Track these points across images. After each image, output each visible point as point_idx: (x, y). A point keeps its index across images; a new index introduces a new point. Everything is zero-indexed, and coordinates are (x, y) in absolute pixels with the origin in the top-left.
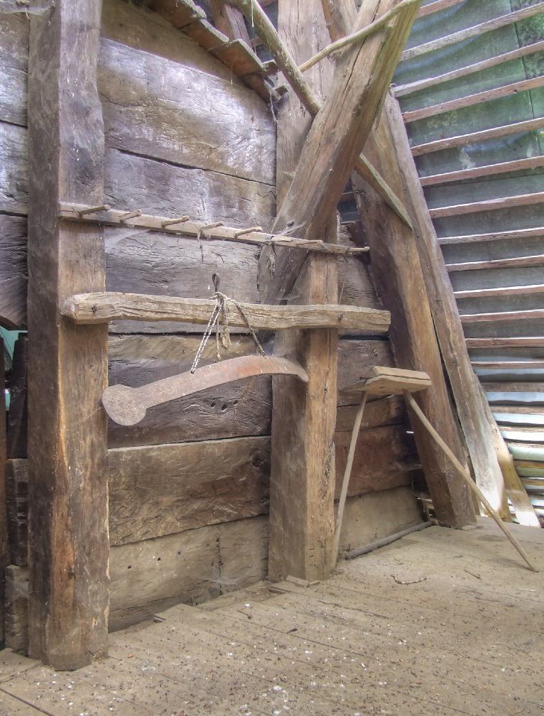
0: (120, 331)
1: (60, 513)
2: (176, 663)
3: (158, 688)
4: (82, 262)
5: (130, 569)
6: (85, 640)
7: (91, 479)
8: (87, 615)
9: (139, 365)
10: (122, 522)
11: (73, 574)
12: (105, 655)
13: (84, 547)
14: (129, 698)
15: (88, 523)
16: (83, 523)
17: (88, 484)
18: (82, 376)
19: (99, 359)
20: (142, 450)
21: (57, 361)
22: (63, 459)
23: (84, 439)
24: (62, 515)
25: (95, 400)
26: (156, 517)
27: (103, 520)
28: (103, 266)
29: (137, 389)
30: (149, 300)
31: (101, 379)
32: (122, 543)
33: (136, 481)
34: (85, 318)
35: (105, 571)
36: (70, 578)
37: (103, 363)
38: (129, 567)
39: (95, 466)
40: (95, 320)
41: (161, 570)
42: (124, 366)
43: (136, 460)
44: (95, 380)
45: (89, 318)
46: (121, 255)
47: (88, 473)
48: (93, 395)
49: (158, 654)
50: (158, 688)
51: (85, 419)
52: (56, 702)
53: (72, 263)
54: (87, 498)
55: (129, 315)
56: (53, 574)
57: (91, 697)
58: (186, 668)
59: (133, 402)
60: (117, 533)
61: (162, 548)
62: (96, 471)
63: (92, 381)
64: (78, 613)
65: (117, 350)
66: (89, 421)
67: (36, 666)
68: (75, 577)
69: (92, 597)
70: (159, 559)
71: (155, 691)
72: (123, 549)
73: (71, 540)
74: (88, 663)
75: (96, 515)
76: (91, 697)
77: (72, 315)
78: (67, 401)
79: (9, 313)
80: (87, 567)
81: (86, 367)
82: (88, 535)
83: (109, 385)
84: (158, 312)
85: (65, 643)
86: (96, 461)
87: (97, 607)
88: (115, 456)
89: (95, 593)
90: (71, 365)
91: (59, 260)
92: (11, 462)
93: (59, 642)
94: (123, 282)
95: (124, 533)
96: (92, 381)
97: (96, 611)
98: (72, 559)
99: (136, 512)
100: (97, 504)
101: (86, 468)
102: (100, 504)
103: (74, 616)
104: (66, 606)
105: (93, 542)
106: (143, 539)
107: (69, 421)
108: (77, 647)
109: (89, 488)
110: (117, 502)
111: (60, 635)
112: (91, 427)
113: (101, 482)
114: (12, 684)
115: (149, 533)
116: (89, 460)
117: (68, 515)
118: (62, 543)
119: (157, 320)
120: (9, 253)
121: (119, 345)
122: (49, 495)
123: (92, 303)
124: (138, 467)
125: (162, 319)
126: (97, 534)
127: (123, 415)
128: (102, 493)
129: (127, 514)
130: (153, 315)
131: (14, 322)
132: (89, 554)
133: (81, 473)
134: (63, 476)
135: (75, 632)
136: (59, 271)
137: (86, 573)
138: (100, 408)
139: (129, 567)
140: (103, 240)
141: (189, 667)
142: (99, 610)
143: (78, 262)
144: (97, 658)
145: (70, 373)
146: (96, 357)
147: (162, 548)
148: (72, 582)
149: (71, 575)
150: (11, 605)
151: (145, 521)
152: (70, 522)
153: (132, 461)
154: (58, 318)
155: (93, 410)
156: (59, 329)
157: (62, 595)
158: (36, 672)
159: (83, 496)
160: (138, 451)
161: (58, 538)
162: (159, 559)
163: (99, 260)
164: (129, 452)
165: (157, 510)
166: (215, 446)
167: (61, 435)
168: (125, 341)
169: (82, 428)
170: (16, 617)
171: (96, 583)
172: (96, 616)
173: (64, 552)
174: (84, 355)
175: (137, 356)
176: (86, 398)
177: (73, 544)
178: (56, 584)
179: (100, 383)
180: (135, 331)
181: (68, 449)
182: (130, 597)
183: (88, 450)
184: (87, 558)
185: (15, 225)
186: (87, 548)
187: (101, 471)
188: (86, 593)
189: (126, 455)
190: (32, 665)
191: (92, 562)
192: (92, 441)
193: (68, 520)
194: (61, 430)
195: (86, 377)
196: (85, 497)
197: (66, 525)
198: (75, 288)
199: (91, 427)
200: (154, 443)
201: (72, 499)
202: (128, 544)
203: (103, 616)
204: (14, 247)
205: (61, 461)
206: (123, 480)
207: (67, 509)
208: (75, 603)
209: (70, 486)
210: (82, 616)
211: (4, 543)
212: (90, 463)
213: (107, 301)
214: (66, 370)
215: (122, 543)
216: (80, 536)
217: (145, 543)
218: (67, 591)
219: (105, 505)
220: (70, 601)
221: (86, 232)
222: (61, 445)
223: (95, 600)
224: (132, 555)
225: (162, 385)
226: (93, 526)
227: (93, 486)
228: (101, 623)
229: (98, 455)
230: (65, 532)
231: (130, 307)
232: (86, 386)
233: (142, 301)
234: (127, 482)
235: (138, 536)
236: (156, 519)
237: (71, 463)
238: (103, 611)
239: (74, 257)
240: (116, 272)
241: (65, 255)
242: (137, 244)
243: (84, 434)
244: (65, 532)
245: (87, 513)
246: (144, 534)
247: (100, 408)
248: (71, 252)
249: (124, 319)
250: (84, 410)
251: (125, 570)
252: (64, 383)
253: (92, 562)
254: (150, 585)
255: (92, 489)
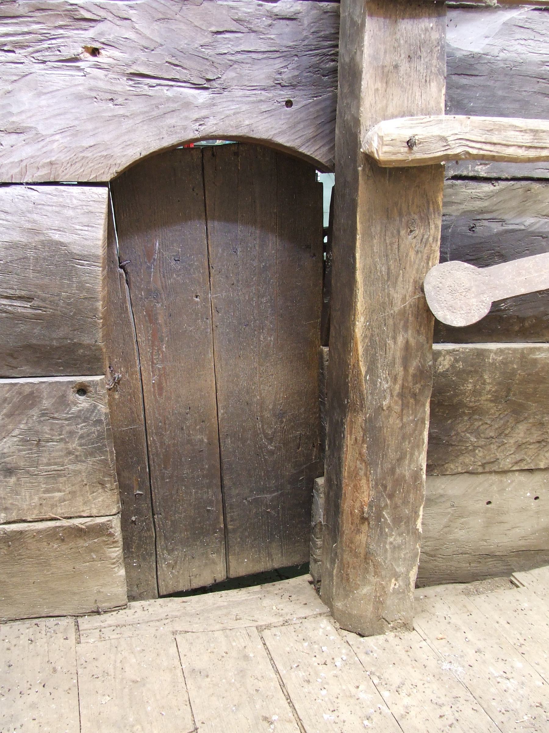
0: (494, 175)
1: (353, 437)
2: (496, 670)
3: (446, 710)
4: (404, 67)
5: (489, 506)
6: (379, 603)
7: (401, 395)
8: (383, 573)
9: (523, 227)
10: (483, 443)
11: (367, 519)
12: (407, 626)
13: (385, 487)
14: (398, 710)
15: (392, 455)
16: (385, 456)
17: (396, 402)
18: (395, 246)
19: (425, 220)
20: (523, 349)
21: (356, 223)
22: (358, 363)
23: (394, 338)
24: (356, 439)
25: (415, 282)
26: (539, 442)
27: (416, 453)
28: (440, 72)
29: (481, 270)
30: (514, 128)
31: (426, 251)
32: (480, 470)
33: (509, 390)
34: (394, 158)
35: (415, 520)
36: (363, 523)
37: (432, 226)
38: (489, 503)
39: (410, 378)
40: (412, 160)
41: (537, 513)
42: (496, 228)
43: (512, 362)
44: (417, 252)
45: (400, 157)
46: (502, 55)
47: (397, 387)
48: (412, 274)
49: (480, 645)
50: (446, 710)
51: (396, 309)
52: (309, 681)
53: (386, 70)
54: (394, 421)
55: (474, 152)
56: (343, 512)
57: (353, 690)
58: (505, 684)
59: (473, 289)
60: (474, 457)
61: (544, 483)
62: (411, 384)
63: (412, 254)
64: (371, 568)
65: (486, 204)
66: (403, 312)
67: (320, 614)
68: (369, 524)
69: (393, 553)
70: (537, 498)
71: (439, 712)
72: (481, 478)
73: (366, 475)
74: (381, 632)
75: (406, 445)
76: (353, 690)
77: (372, 152)
78: (369, 281)
79: (313, 149)
80: (388, 513)
81: (403, 232)
82: (393, 471)
83: (441, 262)
84: (530, 147)
85: (353, 599)
86: (411, 370)
87: (398, 566)
88: (478, 355)
89: (396, 548)
90: (377, 229)
91: (364, 65)
92: (322, 349)
93: (346, 596)
94: (504, 98)
95: (484, 458)
96: (412, 254)
97: (397, 570)
98: (366, 499)
99: (507, 432)
100: (409, 429)
101: (395, 380)
102: (415, 430)
103: (366, 570)
104: (356, 556)
105: (399, 482)
106: (514, 468)
107: (371, 311)
108: (368, 610)
109: (397, 408)
110: (477, 417)
111: (347, 588)
112: (407, 322)
113: (417, 401)
114: (278, 633)
115: (525, 462)
116: (399, 369)
117: (363, 441)
118: (354, 475)
119: (530, 160)
120: (315, 60)
121: (489, 196)
122: (343, 409)
123: (407, 134)
124: (513, 373)
125: (538, 159)
126: (406, 471)
127: (452, 309)
128: (419, 416)
129: (492, 434)
130: (521, 153)
131: (321, 160)
132: (391, 496)
133: (386, 386)
134: (358, 387)
135: (365, 590)
136: (364, 83)
137: (386, 519)
138: (421, 295)
139: (489, 503)
140: (444, 31)
141: (510, 685)
142: (401, 569)
143: (396, 67)
144: (394, 628)
145: (375, 241)
146: (421, 218)
147: (544, 483)
148: (365, 528)
149: (364, 519)
150: (315, 525)
151: (519, 446)
152: (364, 451)
153: (504, 363)
154: (360, 157)
155: (411, 297)
156: (360, 173)
157: (352, 542)
158: (314, 625)
159: (388, 417)
160: (515, 350)
161: (349, 467)
162: (537, 498)
163: (434, 62)
164: (501, 351)
165: (540, 433)
166: (118, 553)
167: (357, 330)
168: (501, 191)
169: (391, 322)
170: (319, 542)
171: (400, 534)
172: (396, 576)
173: (356, 488)
174: (400, 214)
175: (521, 213)
176: (400, 279)
177: (368, 481)
178: (347, 527)
179: (425, 257)
180: (519, 175)
181: (366, 350)
182: (485, 541)
183: (399, 354)
184: (388, 502)
185: (326, 16)
186: (388, 488)
187: (418, 386)
188: (384, 546)
189: (495, 354)
190: (318, 611)
191: (396, 507)
192: (407, 342)
193: (362, 447)
194: (357, 323)
195: (402, 246)
196: (391, 421)
197: (360, 454)
198: (391, 110)
199: (407, 322)
200: (544, 339)
201: (369, 421)
202: (490, 472)
203: (407, 578)
204: (324, 51)
205: (356, 366)
206: (488, 387)
207: (362, 433)
208: (368, 556)
209: (367, 403)
210: (376, 574)
211: (315, 449)
212: (401, 373)
213: (436, 131)
214: (368, 236)
215: (480, 470)
216: (379, 470)
217: (517, 474)
218: (358, 537)
219: (421, 433)
220: (362, 551)
221: (413, 17)
222: (356, 344)
223: (396, 555)
224: (495, 488)
225: (527, 265)
226: (400, 460)
227: (405, 406)
228: (403, 586)
229: (414, 364)
230: (358, 462)
231: (479, 139)
232: (401, 261)
233: (501, 128)
234: (495, 392)
235: (506, 463)
236: (538, 445)
237: (371, 370)
238: (408, 572)
239: (388, 60)
240: (491, 83)
241: (375, 58)
242: (531, 35)
243: (394, 331)
244: (358, 462)
245: (392, 442)
246: (516, 463)
247: (421, 295)
248: (385, 52)
249: (466, 159)
250: (395, 296)
251: (482, 505)
252: (364, 255)
253: (396, 507)
254: (517, 530)
255: (402, 410)
